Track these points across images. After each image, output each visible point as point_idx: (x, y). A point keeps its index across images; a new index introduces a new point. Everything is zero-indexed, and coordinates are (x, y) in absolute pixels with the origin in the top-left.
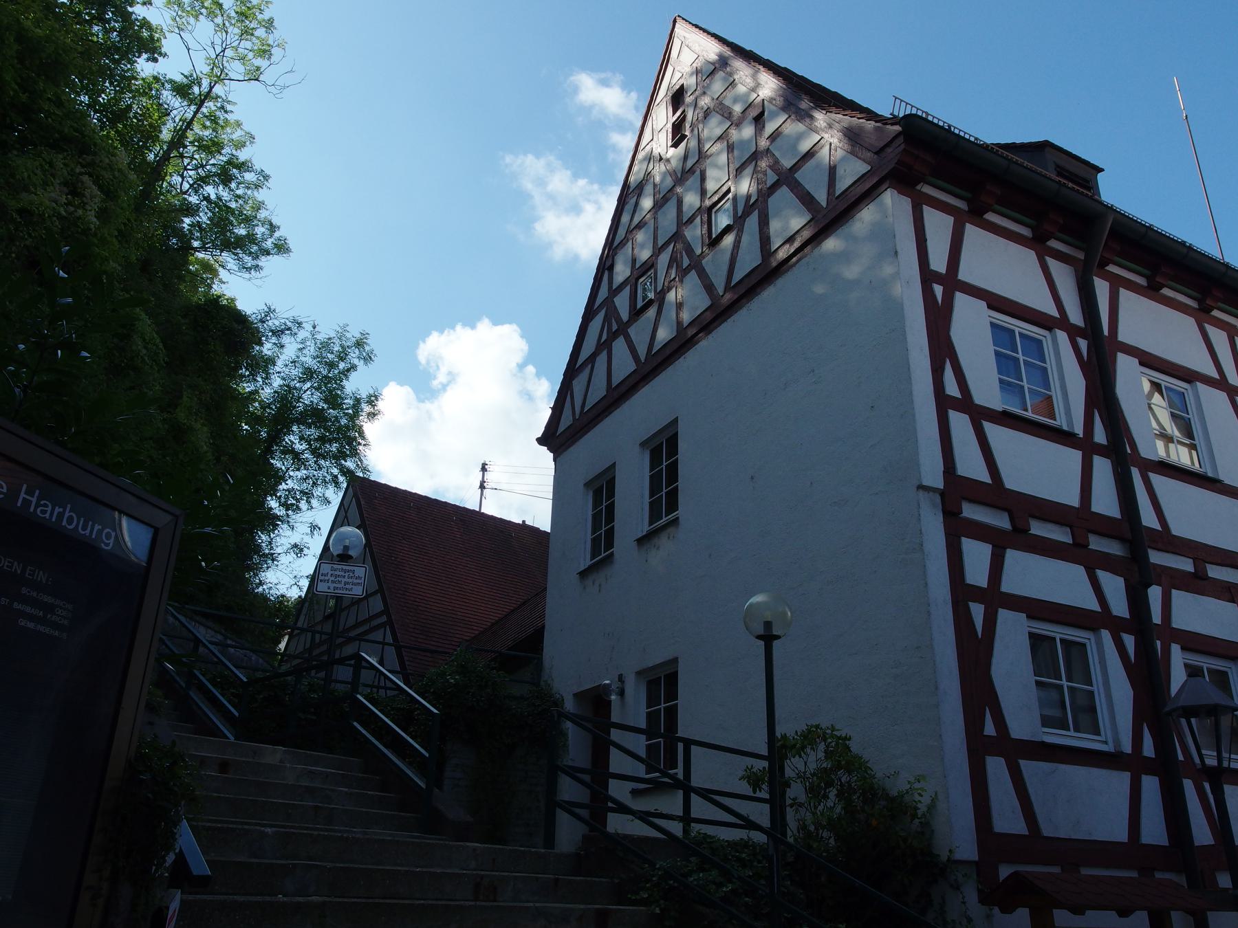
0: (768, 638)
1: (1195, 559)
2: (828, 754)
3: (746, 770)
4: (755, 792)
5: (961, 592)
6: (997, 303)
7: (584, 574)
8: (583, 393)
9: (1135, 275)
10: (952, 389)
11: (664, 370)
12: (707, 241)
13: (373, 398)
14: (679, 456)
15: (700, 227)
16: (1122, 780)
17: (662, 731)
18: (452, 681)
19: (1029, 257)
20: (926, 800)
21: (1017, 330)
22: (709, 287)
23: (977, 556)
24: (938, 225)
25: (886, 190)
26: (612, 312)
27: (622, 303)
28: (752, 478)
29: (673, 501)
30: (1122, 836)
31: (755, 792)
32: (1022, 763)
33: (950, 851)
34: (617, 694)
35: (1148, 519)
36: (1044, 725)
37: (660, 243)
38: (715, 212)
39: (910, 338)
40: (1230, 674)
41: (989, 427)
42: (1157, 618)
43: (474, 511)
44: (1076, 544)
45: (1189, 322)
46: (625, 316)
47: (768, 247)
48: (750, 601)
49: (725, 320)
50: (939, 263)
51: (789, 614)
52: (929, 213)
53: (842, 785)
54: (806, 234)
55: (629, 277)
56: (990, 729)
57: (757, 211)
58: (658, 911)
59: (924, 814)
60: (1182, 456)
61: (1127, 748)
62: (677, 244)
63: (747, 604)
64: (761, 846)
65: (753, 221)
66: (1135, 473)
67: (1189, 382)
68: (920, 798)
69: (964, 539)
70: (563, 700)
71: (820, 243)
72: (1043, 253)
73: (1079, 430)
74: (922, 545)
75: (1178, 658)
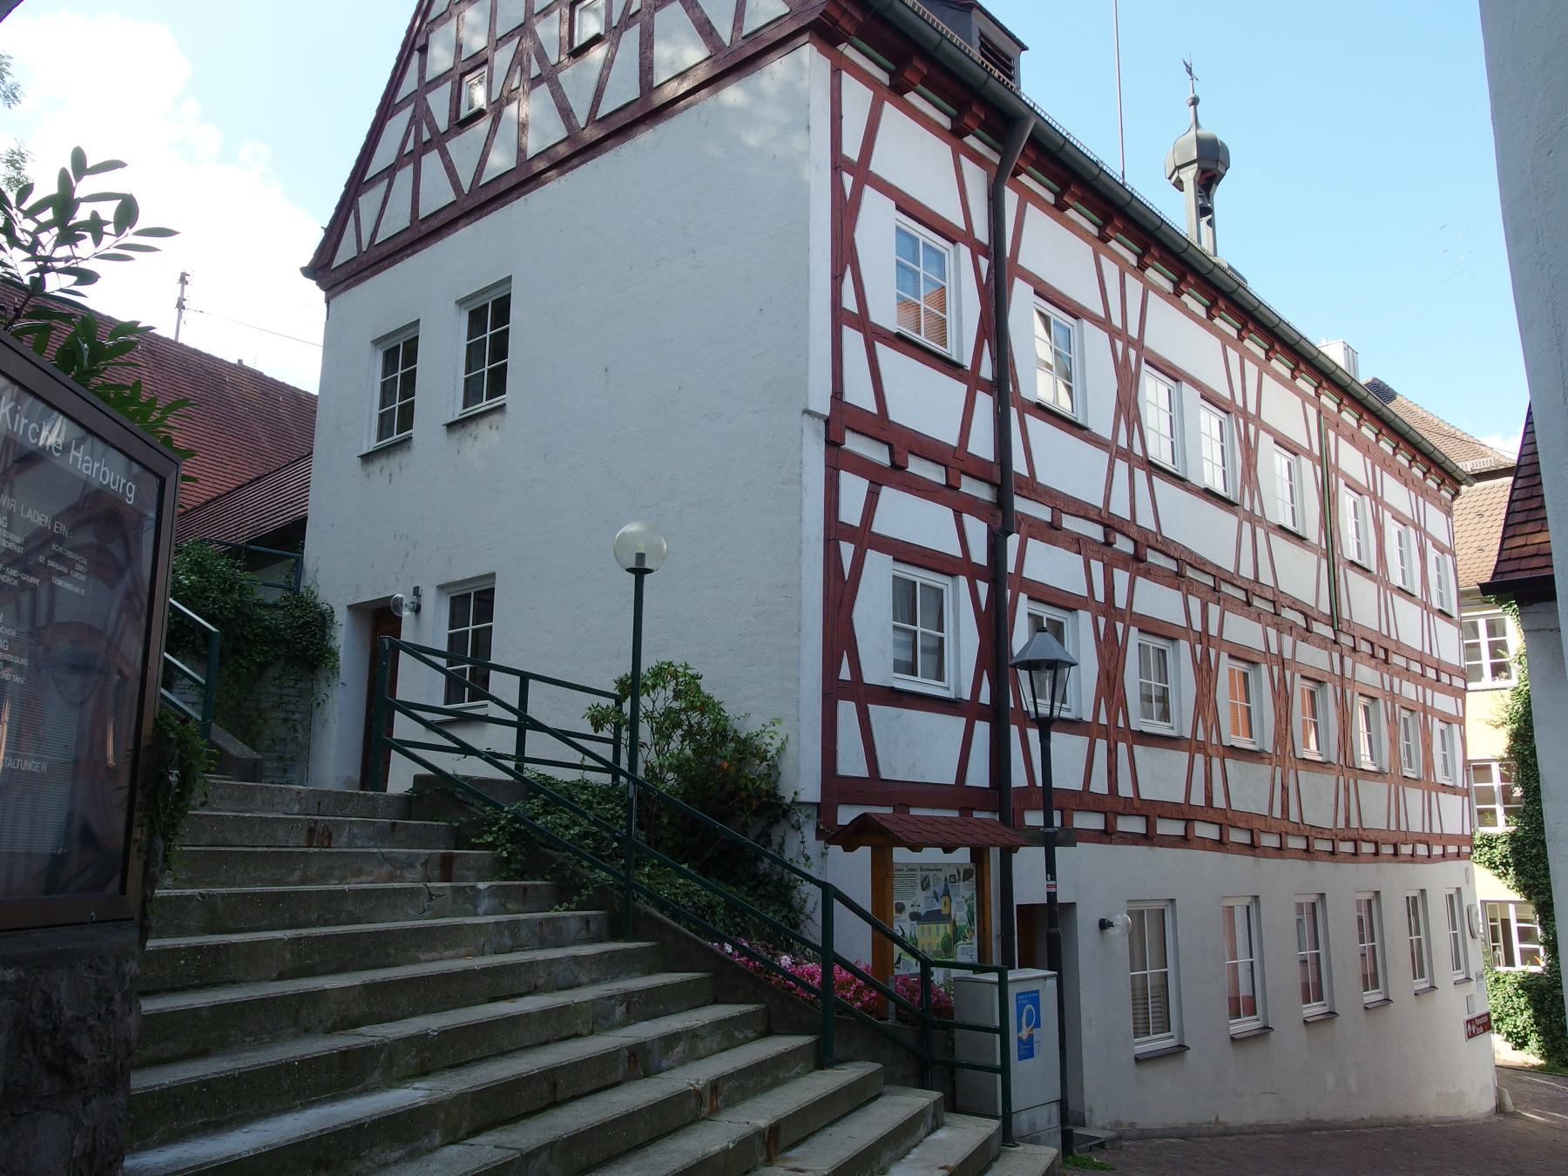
0: (640, 572)
2: (677, 695)
3: (591, 709)
4: (596, 731)
5: (835, 530)
6: (907, 206)
7: (367, 458)
8: (375, 217)
9: (1044, 189)
10: (850, 303)
12: (567, 50)
13: (16, 157)
14: (511, 325)
15: (558, 24)
16: (958, 724)
17: (469, 656)
18: (187, 582)
19: (944, 150)
20: (777, 743)
21: (921, 239)
22: (566, 113)
23: (853, 488)
24: (857, 97)
26: (422, 116)
27: (439, 103)
28: (606, 370)
29: (498, 382)
31: (596, 731)
33: (796, 793)
34: (411, 610)
35: (1019, 465)
36: (895, 671)
37: (500, 33)
38: (580, 10)
40: (1065, 625)
41: (880, 348)
42: (1011, 568)
43: (166, 341)
44: (948, 486)
45: (1085, 250)
46: (442, 124)
48: (623, 530)
50: (851, 149)
51: (665, 546)
52: (847, 80)
53: (690, 726)
54: (702, 75)
55: (450, 70)
56: (845, 674)
58: (505, 854)
59: (772, 757)
61: (967, 695)
62: (523, 41)
64: (600, 787)
65: (632, 36)
66: (1014, 412)
67: (1076, 318)
69: (842, 473)
70: (333, 612)
71: (718, 90)
72: (959, 150)
73: (967, 362)
75: (1024, 606)
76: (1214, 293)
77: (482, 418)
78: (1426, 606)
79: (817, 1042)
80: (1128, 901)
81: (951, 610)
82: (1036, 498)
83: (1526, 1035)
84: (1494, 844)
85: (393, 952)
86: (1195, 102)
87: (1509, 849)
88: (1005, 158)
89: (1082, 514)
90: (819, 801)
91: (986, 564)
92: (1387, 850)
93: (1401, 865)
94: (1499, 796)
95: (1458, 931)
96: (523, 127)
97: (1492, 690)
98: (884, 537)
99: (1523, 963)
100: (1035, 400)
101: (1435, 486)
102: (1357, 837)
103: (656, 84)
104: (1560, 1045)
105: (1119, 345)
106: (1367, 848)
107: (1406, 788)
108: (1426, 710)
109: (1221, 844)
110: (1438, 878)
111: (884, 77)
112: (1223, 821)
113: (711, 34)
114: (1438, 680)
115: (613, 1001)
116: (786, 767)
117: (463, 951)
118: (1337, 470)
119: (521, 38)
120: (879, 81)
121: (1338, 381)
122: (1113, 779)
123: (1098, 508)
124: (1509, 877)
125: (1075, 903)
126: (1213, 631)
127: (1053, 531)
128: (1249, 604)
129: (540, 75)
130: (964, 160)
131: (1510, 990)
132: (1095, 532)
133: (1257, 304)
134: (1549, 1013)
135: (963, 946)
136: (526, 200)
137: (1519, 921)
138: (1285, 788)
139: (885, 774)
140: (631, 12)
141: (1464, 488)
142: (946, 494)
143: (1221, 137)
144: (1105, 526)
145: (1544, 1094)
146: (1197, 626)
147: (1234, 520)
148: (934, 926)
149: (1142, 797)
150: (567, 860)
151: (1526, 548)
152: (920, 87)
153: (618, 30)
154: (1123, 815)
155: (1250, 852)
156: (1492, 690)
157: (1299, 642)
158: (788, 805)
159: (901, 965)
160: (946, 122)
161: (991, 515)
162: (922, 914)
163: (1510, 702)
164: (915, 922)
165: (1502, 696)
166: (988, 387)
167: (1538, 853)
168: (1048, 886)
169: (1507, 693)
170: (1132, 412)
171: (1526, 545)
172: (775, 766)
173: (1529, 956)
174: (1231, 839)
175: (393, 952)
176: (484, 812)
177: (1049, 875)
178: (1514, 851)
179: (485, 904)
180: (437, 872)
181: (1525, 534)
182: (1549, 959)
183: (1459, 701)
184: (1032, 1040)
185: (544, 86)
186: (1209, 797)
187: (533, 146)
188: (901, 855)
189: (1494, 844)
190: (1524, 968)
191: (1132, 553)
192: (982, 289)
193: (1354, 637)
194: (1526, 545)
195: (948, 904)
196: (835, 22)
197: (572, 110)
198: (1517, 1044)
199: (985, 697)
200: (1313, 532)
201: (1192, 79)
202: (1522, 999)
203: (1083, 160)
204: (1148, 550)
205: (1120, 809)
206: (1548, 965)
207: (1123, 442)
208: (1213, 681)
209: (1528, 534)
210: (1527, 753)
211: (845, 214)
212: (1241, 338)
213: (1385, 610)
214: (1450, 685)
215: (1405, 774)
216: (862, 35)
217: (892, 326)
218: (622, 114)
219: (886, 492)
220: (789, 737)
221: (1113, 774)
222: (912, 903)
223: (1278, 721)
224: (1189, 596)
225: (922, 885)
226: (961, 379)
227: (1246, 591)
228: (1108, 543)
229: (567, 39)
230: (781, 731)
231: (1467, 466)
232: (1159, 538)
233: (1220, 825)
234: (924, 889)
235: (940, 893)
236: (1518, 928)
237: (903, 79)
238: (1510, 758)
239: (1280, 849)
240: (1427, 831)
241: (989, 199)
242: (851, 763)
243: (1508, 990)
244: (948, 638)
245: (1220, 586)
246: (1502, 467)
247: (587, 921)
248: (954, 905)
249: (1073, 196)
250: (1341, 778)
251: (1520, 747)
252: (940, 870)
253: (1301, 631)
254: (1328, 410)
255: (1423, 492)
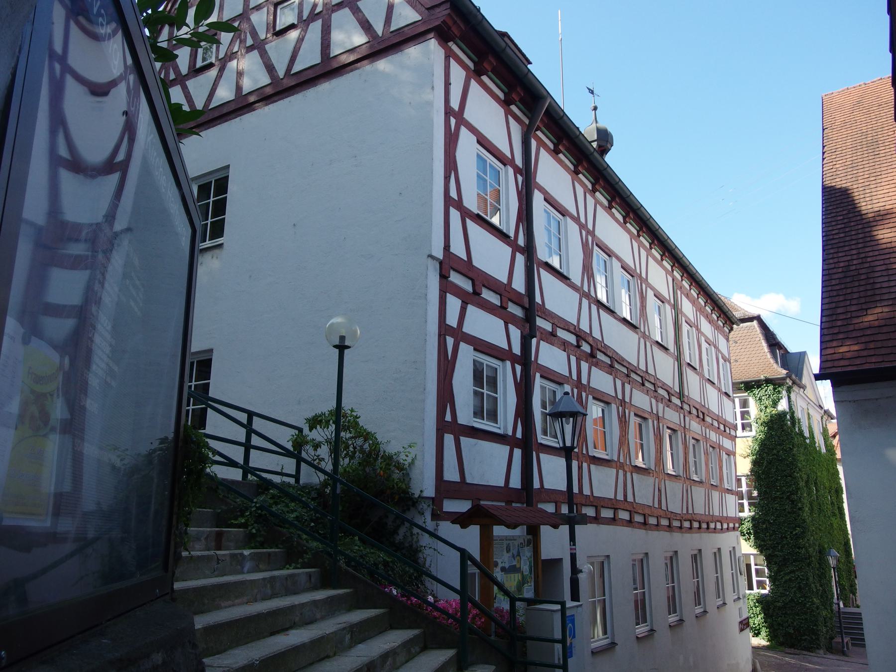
0: (342, 348)
1: (553, 324)
5: (444, 330)
6: (483, 142)
11: (219, 124)
19: (500, 111)
20: (409, 460)
21: (488, 161)
22: (270, 68)
24: (458, 74)
25: (431, 39)
30: (501, 483)
32: (461, 438)
33: (421, 491)
38: (281, 9)
39: (435, 152)
40: (557, 392)
46: (184, 69)
47: (328, 51)
49: (282, 99)
52: (453, 63)
54: (364, 51)
56: (448, 418)
57: (321, 20)
60: (555, 262)
61: (510, 433)
62: (241, 24)
63: (328, 324)
65: (316, 27)
67: (563, 215)
68: (406, 458)
72: (509, 112)
73: (512, 234)
74: (426, 295)
76: (628, 209)
77: (206, 251)
78: (719, 390)
79: (457, 654)
80: (588, 557)
81: (502, 381)
82: (544, 317)
83: (760, 628)
84: (743, 522)
85: (206, 601)
86: (595, 109)
87: (751, 525)
88: (532, 120)
89: (567, 328)
90: (434, 496)
91: (520, 355)
92: (704, 526)
93: (710, 534)
94: (745, 496)
95: (734, 571)
96: (240, 74)
97: (742, 437)
98: (469, 335)
99: (758, 588)
100: (545, 261)
101: (722, 325)
102: (691, 518)
103: (332, 55)
104: (777, 634)
105: (584, 233)
106: (696, 525)
107: (712, 491)
108: (720, 447)
109: (630, 523)
110: (708, 542)
111: (471, 65)
112: (632, 509)
113: (369, 28)
114: (725, 431)
115: (345, 631)
116: (415, 474)
117: (245, 599)
118: (682, 312)
119: (240, 22)
120: (468, 66)
121: (683, 263)
122: (581, 484)
123: (574, 325)
124: (751, 540)
125: (562, 559)
126: (627, 400)
127: (552, 337)
128: (643, 385)
129: (252, 45)
130: (510, 118)
131: (752, 604)
132: (572, 339)
133: (649, 217)
134: (771, 616)
135: (527, 587)
136: (241, 119)
137: (756, 565)
138: (659, 490)
139: (469, 480)
140: (316, 12)
141: (735, 326)
142: (499, 311)
143: (610, 130)
144: (577, 336)
145: (773, 662)
146: (620, 397)
147: (636, 336)
148: (512, 575)
149: (595, 495)
150: (292, 535)
151: (835, 355)
152: (490, 73)
153: (306, 22)
154: (586, 505)
155: (644, 528)
156: (742, 437)
157: (666, 408)
158: (416, 498)
159: (496, 601)
160: (501, 95)
161: (523, 326)
162: (507, 568)
163: (751, 444)
164: (503, 573)
165: (747, 441)
166: (522, 250)
167: (766, 527)
168: (571, 549)
169: (750, 439)
170: (590, 272)
171: (835, 353)
172: (408, 474)
173: (761, 585)
174: (635, 520)
175: (206, 601)
176: (235, 502)
177: (572, 543)
178: (754, 525)
179: (248, 565)
180: (213, 544)
181: (833, 347)
182: (772, 586)
183: (733, 442)
184: (572, 646)
185: (256, 52)
186: (625, 496)
187: (248, 85)
188: (499, 531)
189: (743, 522)
190: (758, 591)
191: (590, 352)
192: (519, 193)
193: (689, 405)
194: (835, 353)
195: (519, 562)
196: (449, 28)
197: (274, 67)
198: (755, 634)
199: (519, 435)
200: (671, 346)
201: (594, 96)
202: (758, 608)
203: (572, 127)
204: (598, 352)
205: (584, 502)
206: (771, 589)
207: (586, 289)
208: (627, 428)
209: (835, 347)
210: (760, 472)
211: (451, 141)
212: (639, 236)
213: (703, 391)
214: (730, 434)
215: (712, 483)
216: (463, 39)
217: (475, 209)
218: (309, 72)
219: (470, 308)
220: (417, 456)
221: (581, 481)
222: (502, 561)
223: (657, 452)
224: (616, 379)
225: (507, 549)
226: (509, 244)
227: (642, 377)
228: (578, 346)
229: (272, 25)
230: (413, 452)
231: (738, 315)
232: (603, 344)
233: (630, 511)
234: (508, 552)
235: (516, 554)
236: (755, 568)
237: (482, 67)
238: (751, 475)
239: (657, 525)
240: (721, 515)
241: (522, 143)
242: (451, 474)
243: (751, 603)
244: (500, 398)
245: (630, 374)
246: (747, 317)
247: (310, 575)
248: (522, 561)
249: (564, 146)
250: (685, 485)
251: (757, 469)
252: (515, 540)
253: (667, 401)
254: (677, 279)
255: (717, 328)
